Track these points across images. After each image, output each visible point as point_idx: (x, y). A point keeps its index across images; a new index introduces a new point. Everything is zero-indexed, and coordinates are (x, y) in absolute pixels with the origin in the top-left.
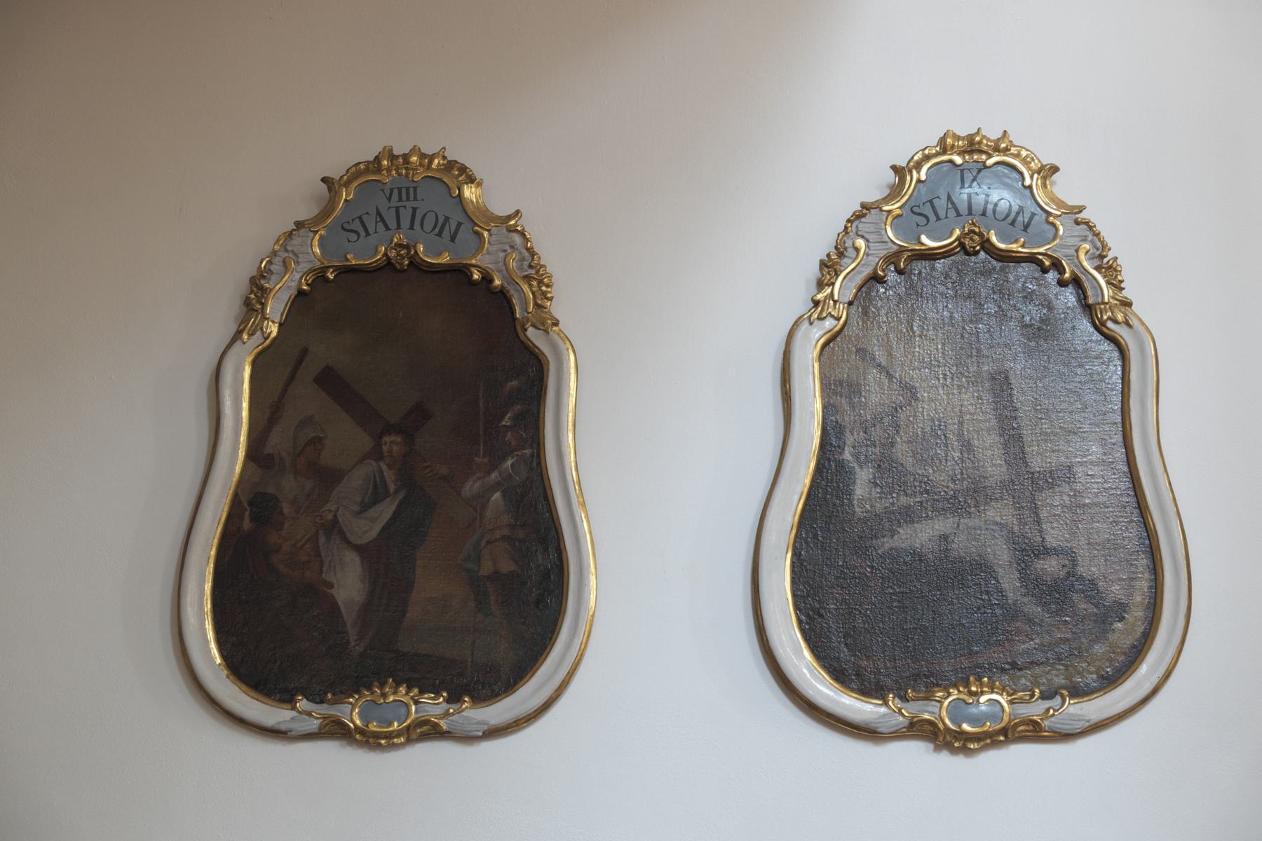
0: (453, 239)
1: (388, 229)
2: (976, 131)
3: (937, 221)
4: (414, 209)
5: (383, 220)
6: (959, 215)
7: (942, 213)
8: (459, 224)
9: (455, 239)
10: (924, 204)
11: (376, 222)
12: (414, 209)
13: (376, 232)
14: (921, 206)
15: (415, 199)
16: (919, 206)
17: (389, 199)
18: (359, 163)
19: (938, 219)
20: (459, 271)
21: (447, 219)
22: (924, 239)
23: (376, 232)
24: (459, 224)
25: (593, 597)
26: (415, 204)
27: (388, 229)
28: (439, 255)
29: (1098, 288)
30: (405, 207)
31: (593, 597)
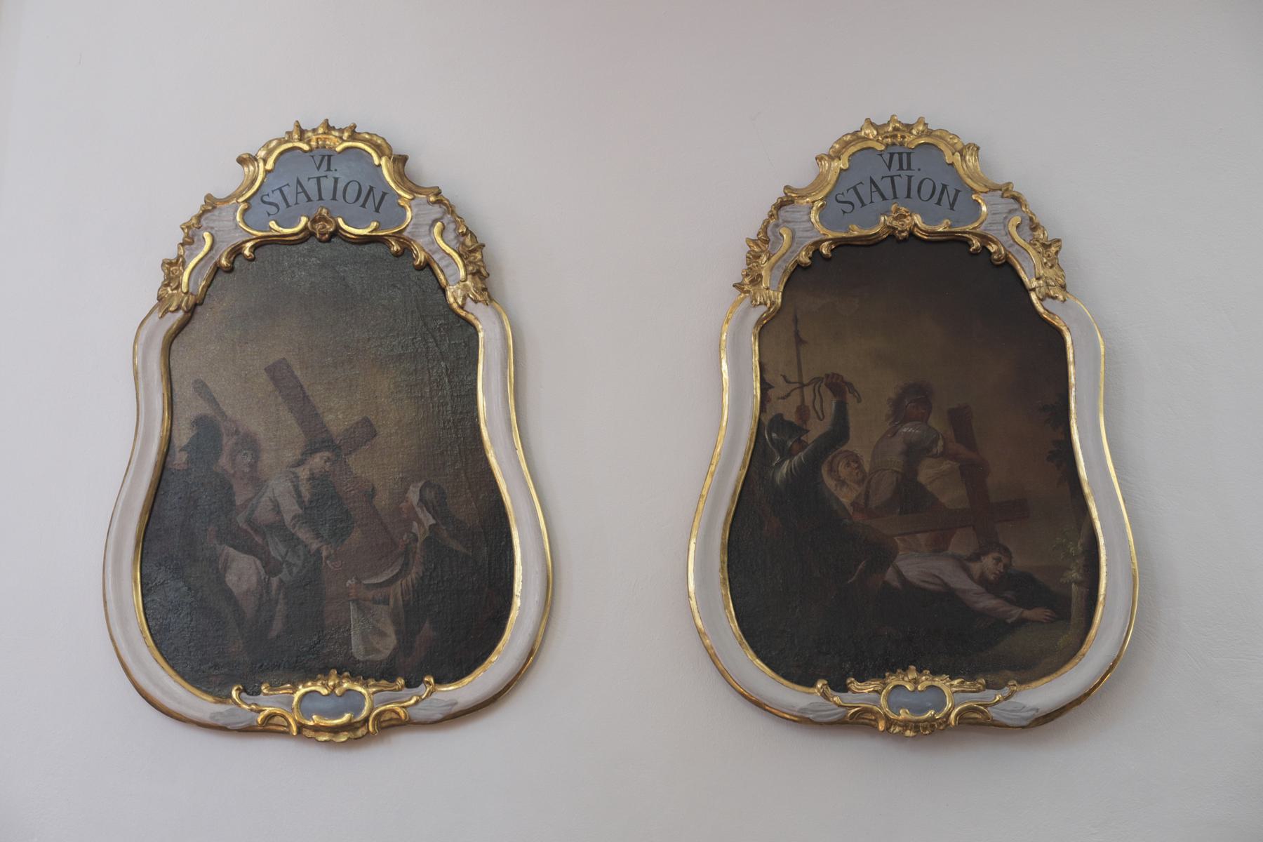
0: (952, 206)
1: (884, 198)
2: (886, 122)
3: (937, 204)
4: (910, 178)
5: (878, 190)
6: (309, 200)
7: (291, 200)
8: (958, 191)
9: (953, 206)
10: (848, 191)
11: (297, 193)
12: (910, 178)
13: (872, 202)
14: (271, 194)
15: (909, 168)
16: (268, 195)
17: (889, 167)
18: (270, 142)
19: (863, 204)
20: (956, 241)
21: (944, 187)
22: (273, 224)
23: (872, 202)
24: (958, 191)
25: (445, 689)
26: (909, 173)
27: (884, 198)
28: (938, 222)
29: (197, 268)
30: (900, 176)
31: (445, 689)
